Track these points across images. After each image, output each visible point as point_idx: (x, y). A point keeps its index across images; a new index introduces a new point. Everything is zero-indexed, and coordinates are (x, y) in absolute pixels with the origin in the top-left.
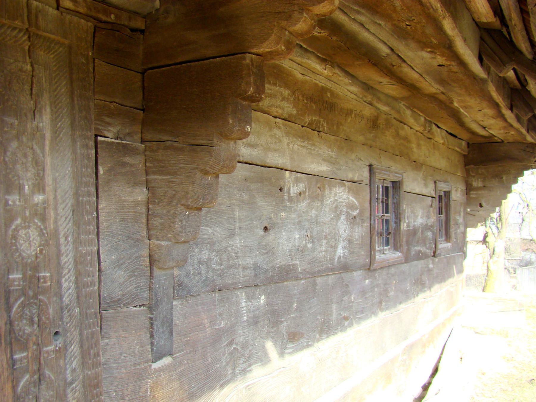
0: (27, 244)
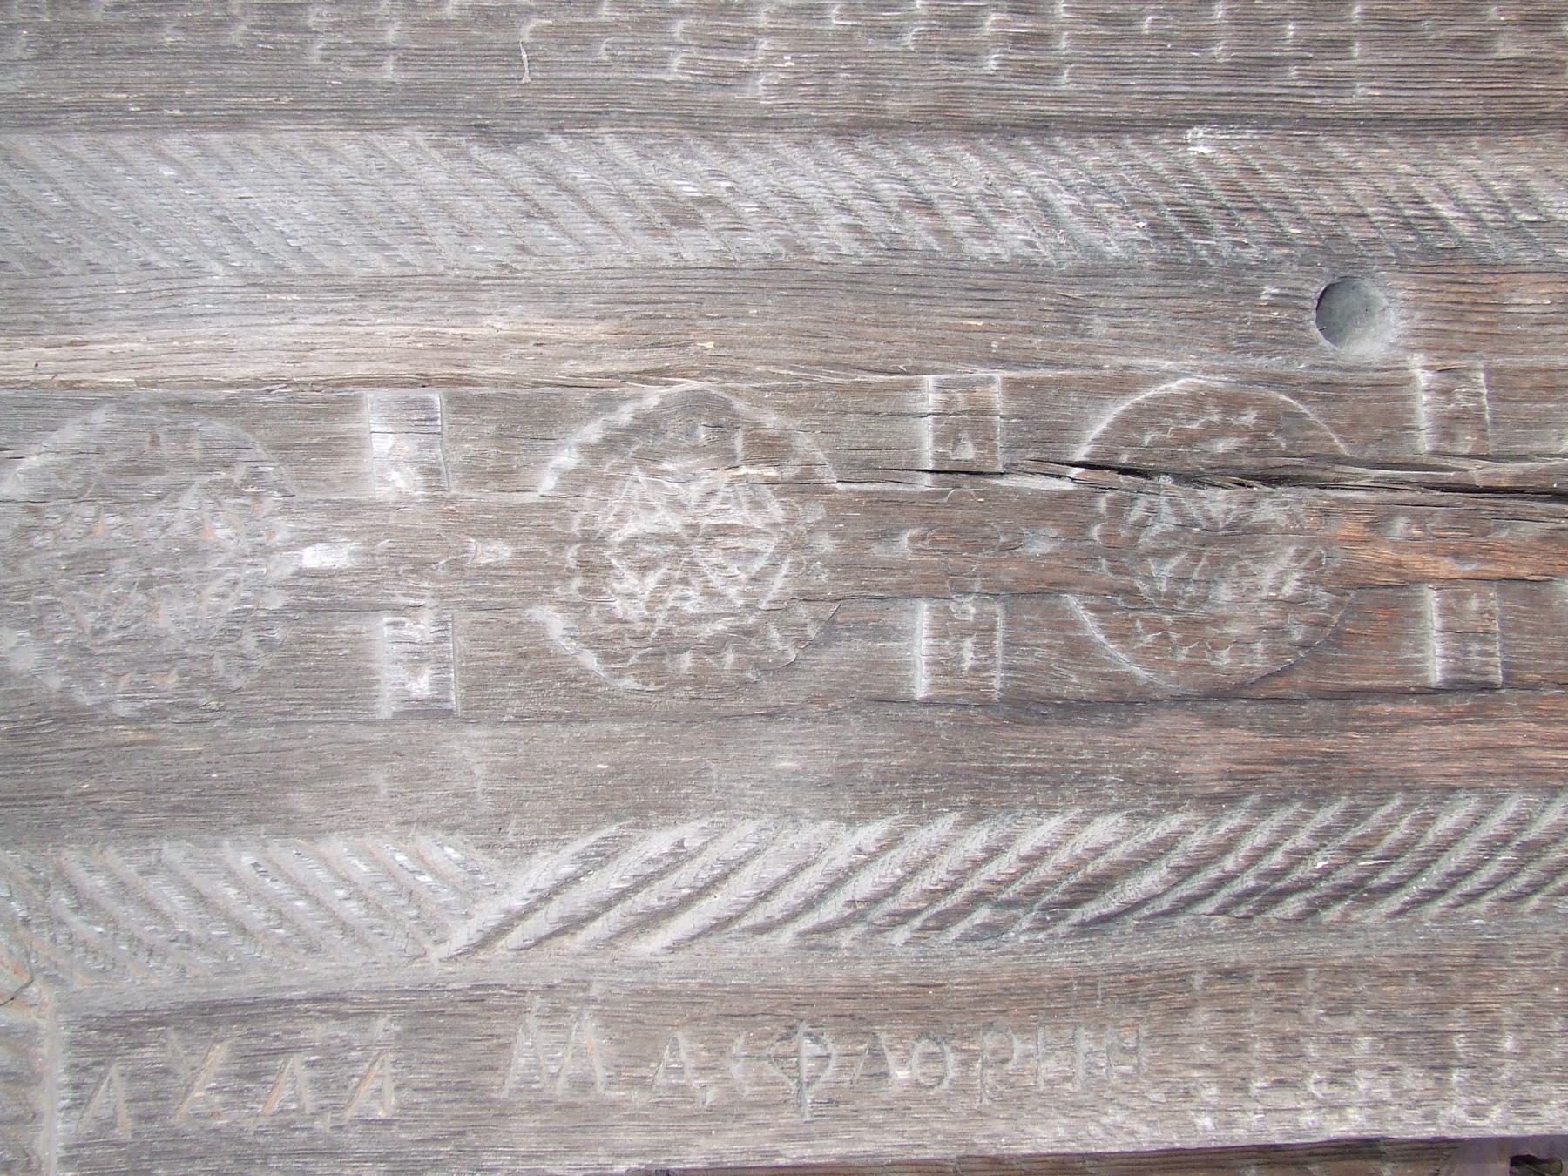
0: (708, 559)
